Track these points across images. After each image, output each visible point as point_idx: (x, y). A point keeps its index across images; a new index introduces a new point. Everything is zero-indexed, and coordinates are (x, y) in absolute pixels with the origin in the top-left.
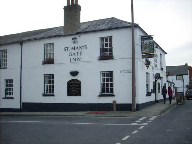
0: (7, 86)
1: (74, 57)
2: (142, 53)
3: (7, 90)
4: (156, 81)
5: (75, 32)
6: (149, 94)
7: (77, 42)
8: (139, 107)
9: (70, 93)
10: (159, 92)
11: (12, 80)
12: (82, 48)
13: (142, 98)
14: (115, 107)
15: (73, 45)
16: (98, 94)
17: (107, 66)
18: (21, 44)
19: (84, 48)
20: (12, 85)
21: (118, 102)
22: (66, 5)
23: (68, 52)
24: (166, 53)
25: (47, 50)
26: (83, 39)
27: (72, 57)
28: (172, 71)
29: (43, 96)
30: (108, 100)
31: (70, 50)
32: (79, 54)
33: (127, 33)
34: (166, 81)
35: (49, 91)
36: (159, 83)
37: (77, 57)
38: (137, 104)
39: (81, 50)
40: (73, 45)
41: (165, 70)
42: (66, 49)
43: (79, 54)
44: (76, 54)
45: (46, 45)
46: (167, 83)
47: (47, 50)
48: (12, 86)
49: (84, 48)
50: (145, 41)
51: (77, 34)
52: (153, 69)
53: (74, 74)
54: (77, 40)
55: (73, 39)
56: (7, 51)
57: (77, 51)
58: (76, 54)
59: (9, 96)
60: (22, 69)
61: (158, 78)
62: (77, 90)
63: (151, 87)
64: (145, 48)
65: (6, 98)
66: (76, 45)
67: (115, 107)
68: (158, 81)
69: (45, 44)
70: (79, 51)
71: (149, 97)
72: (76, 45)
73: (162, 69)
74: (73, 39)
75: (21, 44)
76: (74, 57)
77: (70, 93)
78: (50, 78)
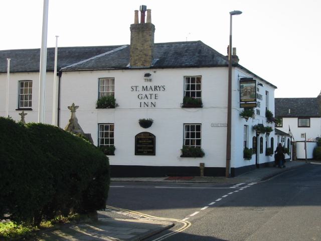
1: (146, 100)
2: (241, 101)
6: (247, 155)
9: (138, 151)
10: (261, 152)
13: (238, 161)
19: (162, 89)
23: (136, 94)
26: (162, 77)
27: (143, 101)
32: (153, 97)
33: (222, 73)
36: (262, 138)
38: (232, 168)
39: (156, 92)
43: (153, 97)
44: (149, 96)
46: (276, 136)
49: (162, 89)
50: (245, 85)
53: (146, 123)
57: (151, 92)
58: (149, 96)
64: (245, 95)
66: (149, 84)
70: (154, 92)
72: (149, 84)
76: (146, 100)
77: (138, 151)
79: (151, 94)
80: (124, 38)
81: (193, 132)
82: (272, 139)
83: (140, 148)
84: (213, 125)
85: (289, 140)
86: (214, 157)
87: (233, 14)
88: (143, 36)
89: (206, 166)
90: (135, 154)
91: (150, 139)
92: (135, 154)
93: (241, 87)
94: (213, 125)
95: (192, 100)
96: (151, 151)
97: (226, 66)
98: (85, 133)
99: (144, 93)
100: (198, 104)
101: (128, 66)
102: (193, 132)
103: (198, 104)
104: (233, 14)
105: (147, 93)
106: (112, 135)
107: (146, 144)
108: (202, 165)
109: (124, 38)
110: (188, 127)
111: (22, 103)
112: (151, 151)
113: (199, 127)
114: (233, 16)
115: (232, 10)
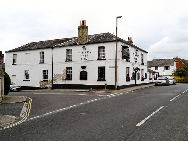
0: (44, 74)
1: (84, 58)
2: (123, 56)
3: (44, 76)
4: (136, 72)
5: (84, 43)
6: (128, 80)
7: (85, 49)
8: (120, 88)
9: (81, 79)
10: (139, 79)
11: (47, 70)
12: (88, 52)
13: (122, 82)
14: (106, 87)
15: (83, 51)
16: (97, 80)
17: (102, 64)
18: (53, 49)
19: (90, 52)
20: (47, 73)
21: (108, 85)
22: (79, 26)
23: (80, 55)
24: (148, 53)
25: (68, 53)
26: (89, 48)
27: (82, 58)
28: (155, 64)
29: (66, 61)
30: (102, 83)
31: (82, 54)
32: (86, 56)
33: (113, 45)
34: (147, 71)
35: (69, 78)
36: (139, 74)
37: (85, 58)
38: (117, 86)
39: (87, 54)
40: (83, 51)
41: (146, 64)
42: (79, 53)
43: (86, 56)
44: (85, 56)
45: (68, 50)
46: (149, 73)
47: (68, 53)
48: (47, 74)
49: (90, 52)
50: (124, 49)
51: (85, 44)
52: (133, 64)
53: (84, 68)
54: (86, 48)
55: (83, 47)
56: (44, 53)
57: (85, 54)
58: (85, 56)
59: (27, 80)
60: (53, 65)
61: (138, 70)
62: (85, 77)
63: (131, 76)
64: (124, 54)
65: (25, 80)
66: (85, 51)
67: (106, 87)
68: (138, 72)
69: (67, 50)
70: (87, 54)
71: (143, 81)
72: (85, 51)
73: (143, 64)
74: (83, 47)
75: (53, 49)
76: (84, 58)
77: (81, 79)
78: (69, 70)
79: (85, 56)
80: (75, 34)
81: (102, 70)
82: (146, 74)
83: (82, 77)
84: (110, 67)
85: (157, 75)
86: (110, 81)
87: (117, 18)
88: (83, 31)
89: (107, 85)
90: (80, 80)
91: (85, 74)
92: (80, 80)
93: (123, 50)
94: (110, 67)
95: (102, 57)
96: (86, 79)
97: (115, 41)
98: (6, 71)
99: (83, 54)
100: (104, 59)
101: (77, 44)
102: (102, 70)
103: (104, 59)
104: (117, 18)
105: (84, 54)
106: (104, 72)
107: (84, 75)
108: (106, 84)
109: (75, 34)
110: (44, 71)
111: (44, 78)
112: (86, 79)
113: (104, 68)
114: (118, 19)
115: (117, 16)
